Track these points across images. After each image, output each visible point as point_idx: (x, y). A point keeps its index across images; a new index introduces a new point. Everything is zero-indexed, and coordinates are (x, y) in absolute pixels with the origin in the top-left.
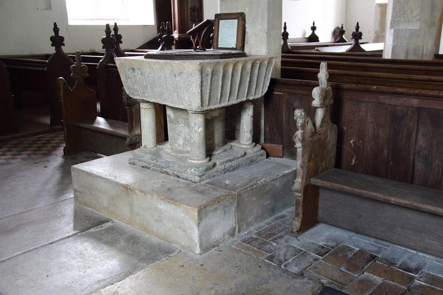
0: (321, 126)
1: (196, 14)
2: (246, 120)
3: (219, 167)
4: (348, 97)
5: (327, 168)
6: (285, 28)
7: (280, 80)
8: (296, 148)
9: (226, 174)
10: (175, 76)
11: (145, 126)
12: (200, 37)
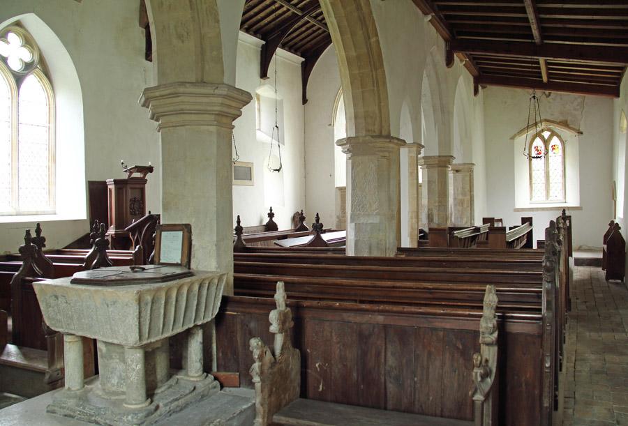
0: (282, 354)
1: (136, 206)
2: (195, 348)
3: (163, 409)
4: (310, 316)
5: (291, 400)
6: (239, 222)
7: (232, 297)
8: (254, 383)
9: (172, 417)
10: (108, 306)
11: (69, 363)
12: (140, 233)
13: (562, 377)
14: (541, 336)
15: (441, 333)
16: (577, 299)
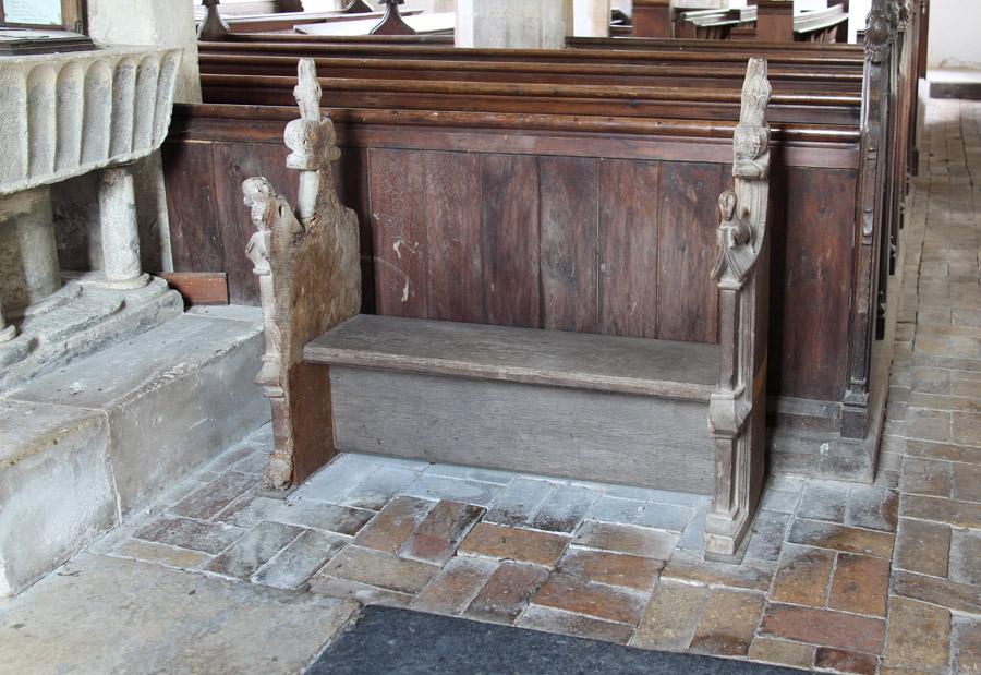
2: (117, 216)
3: (46, 348)
5: (342, 318)
7: (199, 108)
8: (258, 276)
9: (72, 365)
13: (893, 284)
14: (856, 173)
15: (654, 171)
16: (931, 155)
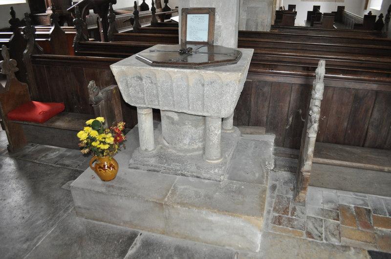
10: (203, 85)
